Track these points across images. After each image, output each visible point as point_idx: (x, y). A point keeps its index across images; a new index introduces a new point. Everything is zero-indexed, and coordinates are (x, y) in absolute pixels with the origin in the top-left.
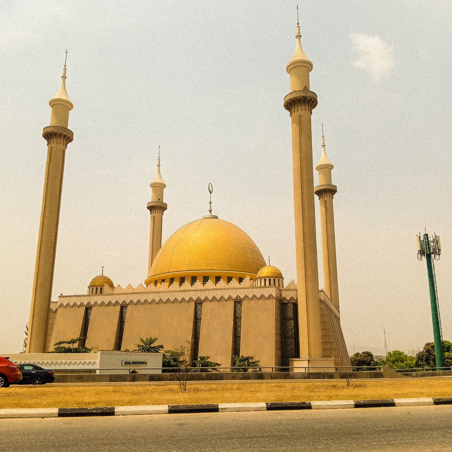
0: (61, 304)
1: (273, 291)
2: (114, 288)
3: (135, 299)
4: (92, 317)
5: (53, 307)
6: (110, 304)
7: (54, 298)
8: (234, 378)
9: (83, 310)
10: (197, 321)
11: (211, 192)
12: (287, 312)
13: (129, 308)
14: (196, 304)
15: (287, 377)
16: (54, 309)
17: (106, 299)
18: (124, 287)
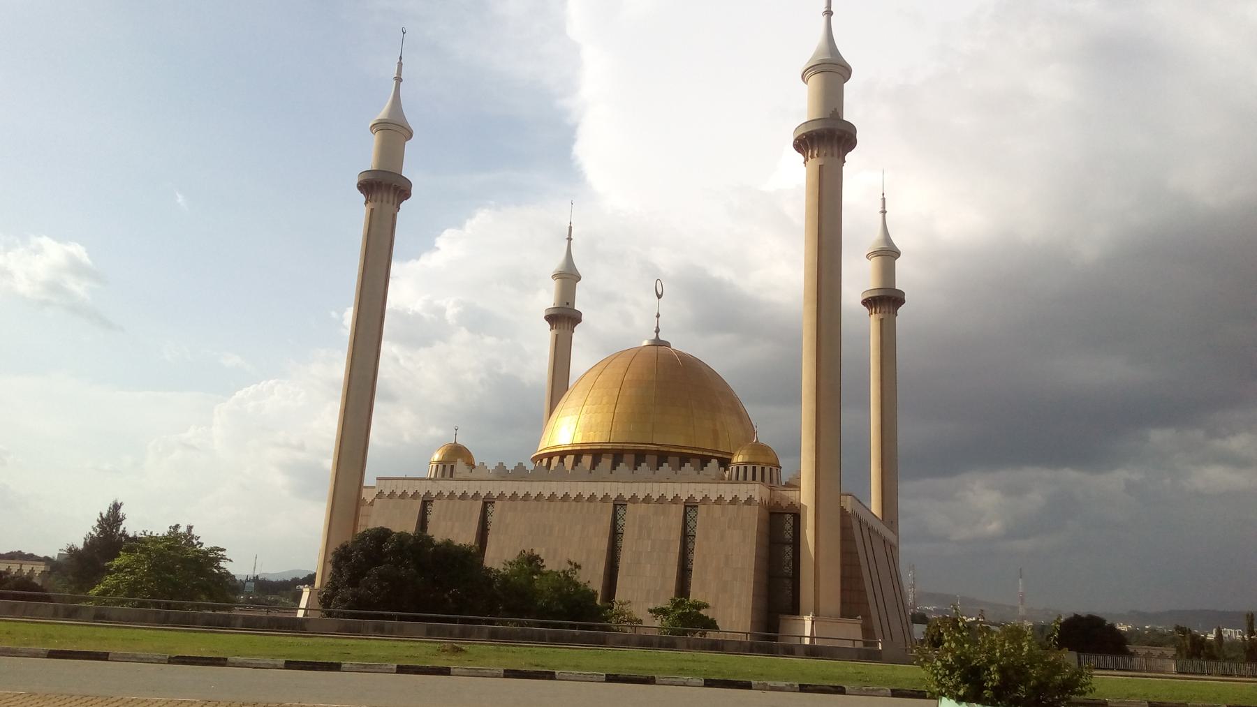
0: (381, 492)
1: (757, 491)
2: (474, 467)
3: (508, 488)
4: (493, 519)
5: (368, 496)
6: (464, 496)
7: (369, 479)
8: (671, 645)
9: (418, 504)
10: (686, 537)
11: (659, 297)
12: (779, 527)
13: (498, 504)
14: (615, 506)
15: (771, 651)
16: (369, 500)
17: (458, 487)
18: (491, 466)
